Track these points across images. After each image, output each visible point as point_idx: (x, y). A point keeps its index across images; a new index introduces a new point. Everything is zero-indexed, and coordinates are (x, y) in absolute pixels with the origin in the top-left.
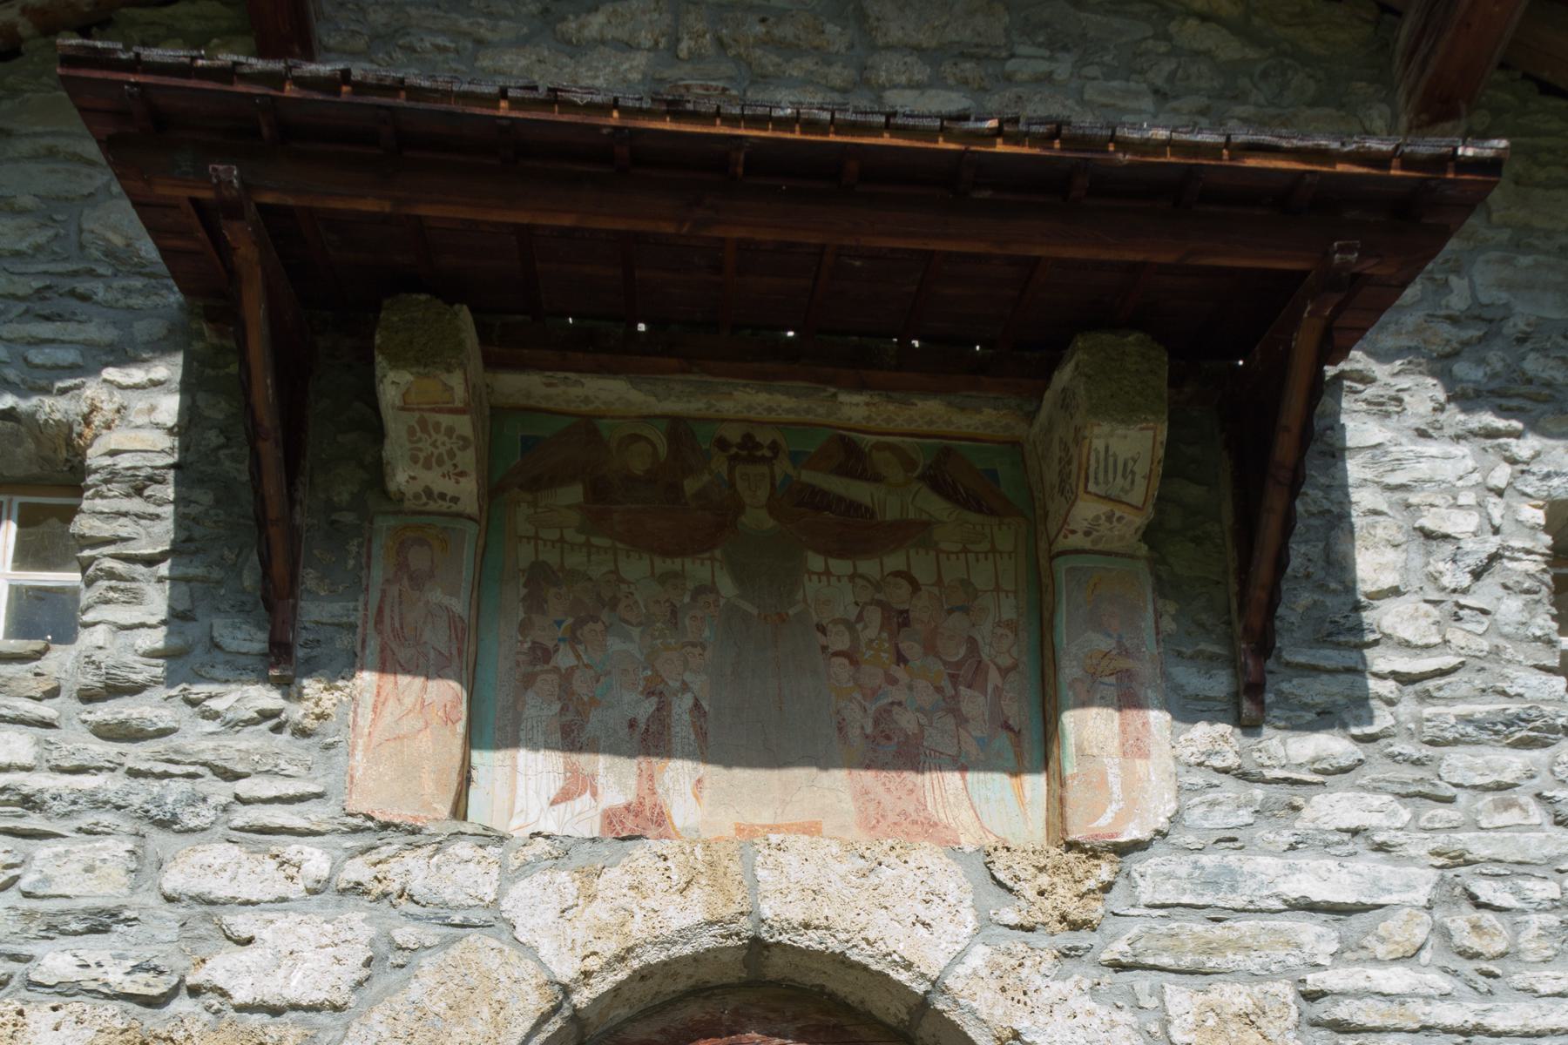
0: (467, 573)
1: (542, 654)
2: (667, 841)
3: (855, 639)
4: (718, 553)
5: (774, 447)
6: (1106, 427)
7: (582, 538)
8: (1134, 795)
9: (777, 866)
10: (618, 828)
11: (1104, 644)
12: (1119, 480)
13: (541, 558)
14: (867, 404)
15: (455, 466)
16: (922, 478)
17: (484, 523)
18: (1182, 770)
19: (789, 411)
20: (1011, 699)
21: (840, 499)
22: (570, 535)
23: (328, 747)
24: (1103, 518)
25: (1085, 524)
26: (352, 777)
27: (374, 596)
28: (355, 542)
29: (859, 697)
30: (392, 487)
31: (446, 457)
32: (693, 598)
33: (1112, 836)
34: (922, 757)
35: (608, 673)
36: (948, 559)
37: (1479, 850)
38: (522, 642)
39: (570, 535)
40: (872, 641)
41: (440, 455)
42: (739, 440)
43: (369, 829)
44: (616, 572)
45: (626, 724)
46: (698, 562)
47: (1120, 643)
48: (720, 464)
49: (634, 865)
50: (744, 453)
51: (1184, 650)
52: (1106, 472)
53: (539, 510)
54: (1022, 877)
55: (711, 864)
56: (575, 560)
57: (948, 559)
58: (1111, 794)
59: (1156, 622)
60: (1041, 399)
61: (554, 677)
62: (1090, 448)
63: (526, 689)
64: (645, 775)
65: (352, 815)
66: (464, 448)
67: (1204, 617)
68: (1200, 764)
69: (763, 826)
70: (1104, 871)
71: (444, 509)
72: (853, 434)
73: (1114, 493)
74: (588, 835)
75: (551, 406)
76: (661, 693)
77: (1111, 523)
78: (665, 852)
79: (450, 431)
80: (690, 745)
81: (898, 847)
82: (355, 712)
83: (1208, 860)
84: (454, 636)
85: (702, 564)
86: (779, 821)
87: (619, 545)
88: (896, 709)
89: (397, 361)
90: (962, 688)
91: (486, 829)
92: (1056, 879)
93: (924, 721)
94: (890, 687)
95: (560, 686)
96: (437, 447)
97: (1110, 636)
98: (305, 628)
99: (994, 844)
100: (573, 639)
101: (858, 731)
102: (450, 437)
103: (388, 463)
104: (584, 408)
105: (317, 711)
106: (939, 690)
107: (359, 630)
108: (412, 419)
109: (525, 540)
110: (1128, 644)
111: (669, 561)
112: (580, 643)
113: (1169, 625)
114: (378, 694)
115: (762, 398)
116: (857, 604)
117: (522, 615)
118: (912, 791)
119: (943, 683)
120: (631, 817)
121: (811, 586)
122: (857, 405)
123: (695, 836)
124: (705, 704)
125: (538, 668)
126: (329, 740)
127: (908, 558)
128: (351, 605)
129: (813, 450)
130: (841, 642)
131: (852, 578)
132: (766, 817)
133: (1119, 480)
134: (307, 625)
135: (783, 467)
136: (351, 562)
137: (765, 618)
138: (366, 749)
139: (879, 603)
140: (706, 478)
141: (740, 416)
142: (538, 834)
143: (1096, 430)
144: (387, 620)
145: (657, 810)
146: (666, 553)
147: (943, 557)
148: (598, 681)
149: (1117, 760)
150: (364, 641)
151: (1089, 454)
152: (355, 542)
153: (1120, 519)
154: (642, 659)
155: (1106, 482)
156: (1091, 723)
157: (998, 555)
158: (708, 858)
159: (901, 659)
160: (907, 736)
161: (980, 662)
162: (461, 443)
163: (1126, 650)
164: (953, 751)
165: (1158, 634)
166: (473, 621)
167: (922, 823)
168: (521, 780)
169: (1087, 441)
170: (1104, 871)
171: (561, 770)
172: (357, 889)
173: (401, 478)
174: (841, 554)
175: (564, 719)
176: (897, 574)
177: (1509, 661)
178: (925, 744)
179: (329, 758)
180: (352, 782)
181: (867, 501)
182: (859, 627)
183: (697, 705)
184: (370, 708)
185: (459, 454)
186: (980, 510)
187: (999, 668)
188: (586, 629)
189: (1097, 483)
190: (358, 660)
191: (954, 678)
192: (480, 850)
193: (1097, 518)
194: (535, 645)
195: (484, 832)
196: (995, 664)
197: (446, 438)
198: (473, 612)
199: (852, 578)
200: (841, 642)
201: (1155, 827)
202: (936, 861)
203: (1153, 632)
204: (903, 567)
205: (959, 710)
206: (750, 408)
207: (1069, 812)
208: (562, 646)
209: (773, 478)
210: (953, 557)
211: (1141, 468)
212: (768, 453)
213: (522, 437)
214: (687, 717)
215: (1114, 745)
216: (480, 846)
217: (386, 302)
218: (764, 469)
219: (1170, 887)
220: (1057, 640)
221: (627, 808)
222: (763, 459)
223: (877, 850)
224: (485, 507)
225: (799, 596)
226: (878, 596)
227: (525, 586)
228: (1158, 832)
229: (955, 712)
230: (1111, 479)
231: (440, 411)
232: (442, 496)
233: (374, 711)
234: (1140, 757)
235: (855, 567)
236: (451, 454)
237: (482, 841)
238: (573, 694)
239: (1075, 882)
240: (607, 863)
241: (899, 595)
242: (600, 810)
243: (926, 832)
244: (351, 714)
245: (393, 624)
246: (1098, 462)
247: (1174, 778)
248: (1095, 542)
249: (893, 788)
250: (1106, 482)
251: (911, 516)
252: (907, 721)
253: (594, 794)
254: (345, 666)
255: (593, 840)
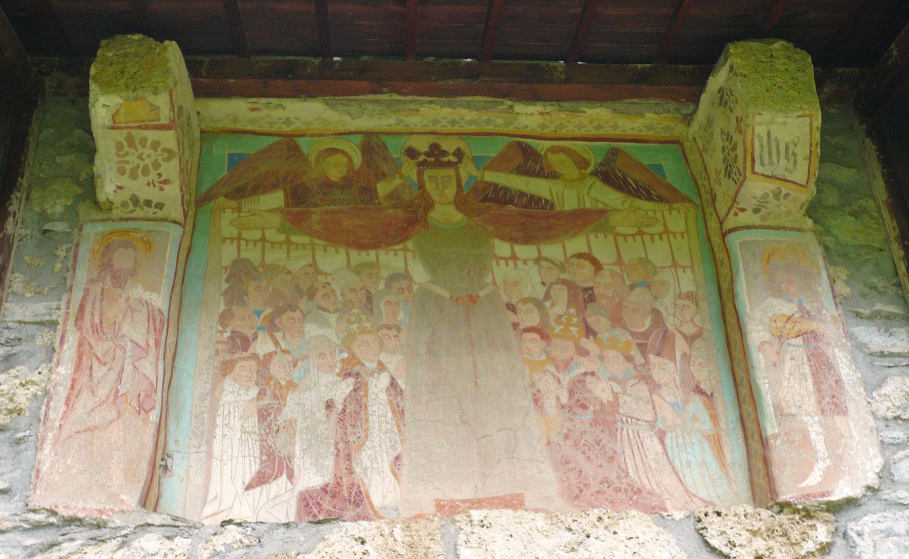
0: (169, 270)
1: (241, 342)
2: (365, 523)
3: (544, 315)
4: (410, 244)
5: (459, 153)
6: (766, 116)
7: (282, 237)
8: (839, 451)
9: (481, 543)
10: (315, 510)
11: (788, 308)
12: (783, 161)
13: (243, 256)
14: (541, 114)
15: (160, 175)
16: (595, 174)
17: (189, 227)
18: (881, 425)
19: (471, 122)
20: (700, 364)
21: (522, 194)
22: (271, 235)
23: (18, 442)
24: (771, 195)
25: (755, 202)
26: (38, 471)
27: (77, 296)
28: (64, 247)
29: (553, 369)
30: (101, 197)
31: (151, 168)
32: (388, 286)
33: (823, 495)
34: (619, 424)
35: (305, 357)
36: (626, 241)
38: (222, 333)
39: (271, 235)
40: (560, 317)
41: (146, 166)
42: (426, 149)
43: (52, 524)
44: (314, 265)
45: (323, 406)
46: (392, 253)
47: (801, 307)
48: (410, 170)
49: (329, 550)
50: (432, 159)
51: (861, 310)
52: (770, 154)
53: (242, 215)
54: (737, 543)
55: (411, 546)
56: (274, 257)
57: (626, 241)
58: (816, 452)
59: (832, 287)
60: (696, 101)
61: (253, 363)
62: (753, 135)
63: (224, 376)
64: (342, 455)
65: (34, 511)
66: (168, 159)
67: (875, 280)
68: (897, 418)
69: (464, 501)
70: (822, 533)
71: (150, 215)
72: (530, 141)
73: (780, 173)
74: (284, 520)
75: (256, 128)
76: (358, 374)
77: (778, 199)
78: (362, 535)
79: (155, 145)
80: (387, 422)
81: (605, 518)
82: (48, 406)
84: (152, 328)
85: (396, 255)
86: (481, 495)
87: (317, 241)
88: (589, 378)
89: (108, 87)
90: (651, 357)
91: (176, 519)
92: (771, 543)
93: (618, 389)
94: (581, 359)
95: (258, 372)
96: (143, 160)
97: (790, 301)
98: (8, 328)
99: (704, 510)
100: (271, 327)
101: (553, 402)
102: (156, 150)
103: (99, 176)
104: (286, 129)
105: (11, 406)
106: (629, 359)
107: (59, 327)
108: (121, 136)
109: (228, 241)
110: (808, 307)
111: (364, 253)
112: (278, 330)
113: (843, 289)
114: (72, 387)
115: (446, 112)
116: (543, 284)
117: (222, 307)
118: (612, 458)
119: (632, 353)
120: (328, 498)
121: (500, 271)
122: (532, 114)
123: (394, 515)
124: (401, 383)
125: (237, 355)
126: (20, 435)
127: (588, 242)
128: (54, 304)
129: (493, 155)
130: (531, 319)
131: (537, 261)
132: (467, 492)
133: (783, 161)
134: (10, 325)
135: (467, 170)
136: (58, 266)
137: (457, 300)
138: (56, 440)
139: (565, 282)
140: (397, 181)
141: (427, 129)
142: (230, 522)
143: (758, 118)
144: (87, 316)
145: (355, 490)
146: (361, 246)
147: (620, 240)
148: (295, 366)
149: (816, 419)
150: (63, 338)
151: (753, 140)
152: (64, 247)
153: (787, 195)
154: (339, 342)
155: (771, 164)
156: (785, 383)
157: (671, 236)
158: (408, 539)
159: (589, 332)
160: (602, 404)
161: (666, 331)
162: (166, 155)
163: (808, 313)
164: (649, 416)
165: (834, 297)
166: (174, 314)
167: (626, 491)
168: (215, 463)
169: (750, 128)
170: (822, 533)
171: (258, 454)
173: (107, 190)
174: (527, 240)
175: (261, 403)
176: (580, 256)
178: (621, 411)
179: (18, 453)
180: (37, 477)
181: (546, 195)
182: (548, 304)
183: (393, 384)
184: (62, 402)
185: (164, 165)
186: (650, 198)
187: (685, 337)
188: (284, 317)
189: (763, 165)
190: (55, 355)
191: (642, 347)
192: (167, 542)
193: (766, 195)
194: (235, 335)
195: (173, 523)
196: (680, 332)
197: (152, 152)
198: (174, 307)
199: (537, 261)
200: (531, 319)
201: (865, 483)
202: (646, 530)
203: (830, 296)
204: (585, 250)
205: (651, 377)
206: (436, 122)
207: (776, 472)
208: (261, 334)
209: (459, 179)
210: (630, 239)
211: (802, 151)
212: (453, 159)
213: (229, 154)
214: (383, 396)
215: (810, 403)
216: (168, 538)
217: (103, 42)
218: (450, 172)
219: (891, 545)
220: (740, 308)
221: (324, 489)
222: (449, 164)
223: (584, 521)
224: (191, 213)
225: (489, 279)
226: (563, 276)
227: (227, 281)
228: (869, 488)
229: (647, 379)
230: (775, 161)
231: (147, 128)
232: (148, 203)
233: (67, 403)
234: (839, 413)
235: (539, 252)
236: (156, 165)
237: (169, 532)
238: (270, 379)
239: (793, 544)
240: (301, 549)
241: (583, 274)
242: (296, 493)
243: (631, 499)
244: (44, 408)
245: (92, 320)
246: (762, 146)
247: (875, 432)
248: (763, 218)
249: (592, 456)
250: (771, 164)
251: (588, 205)
252: (601, 390)
253: (291, 477)
254: (44, 362)
255: (287, 525)
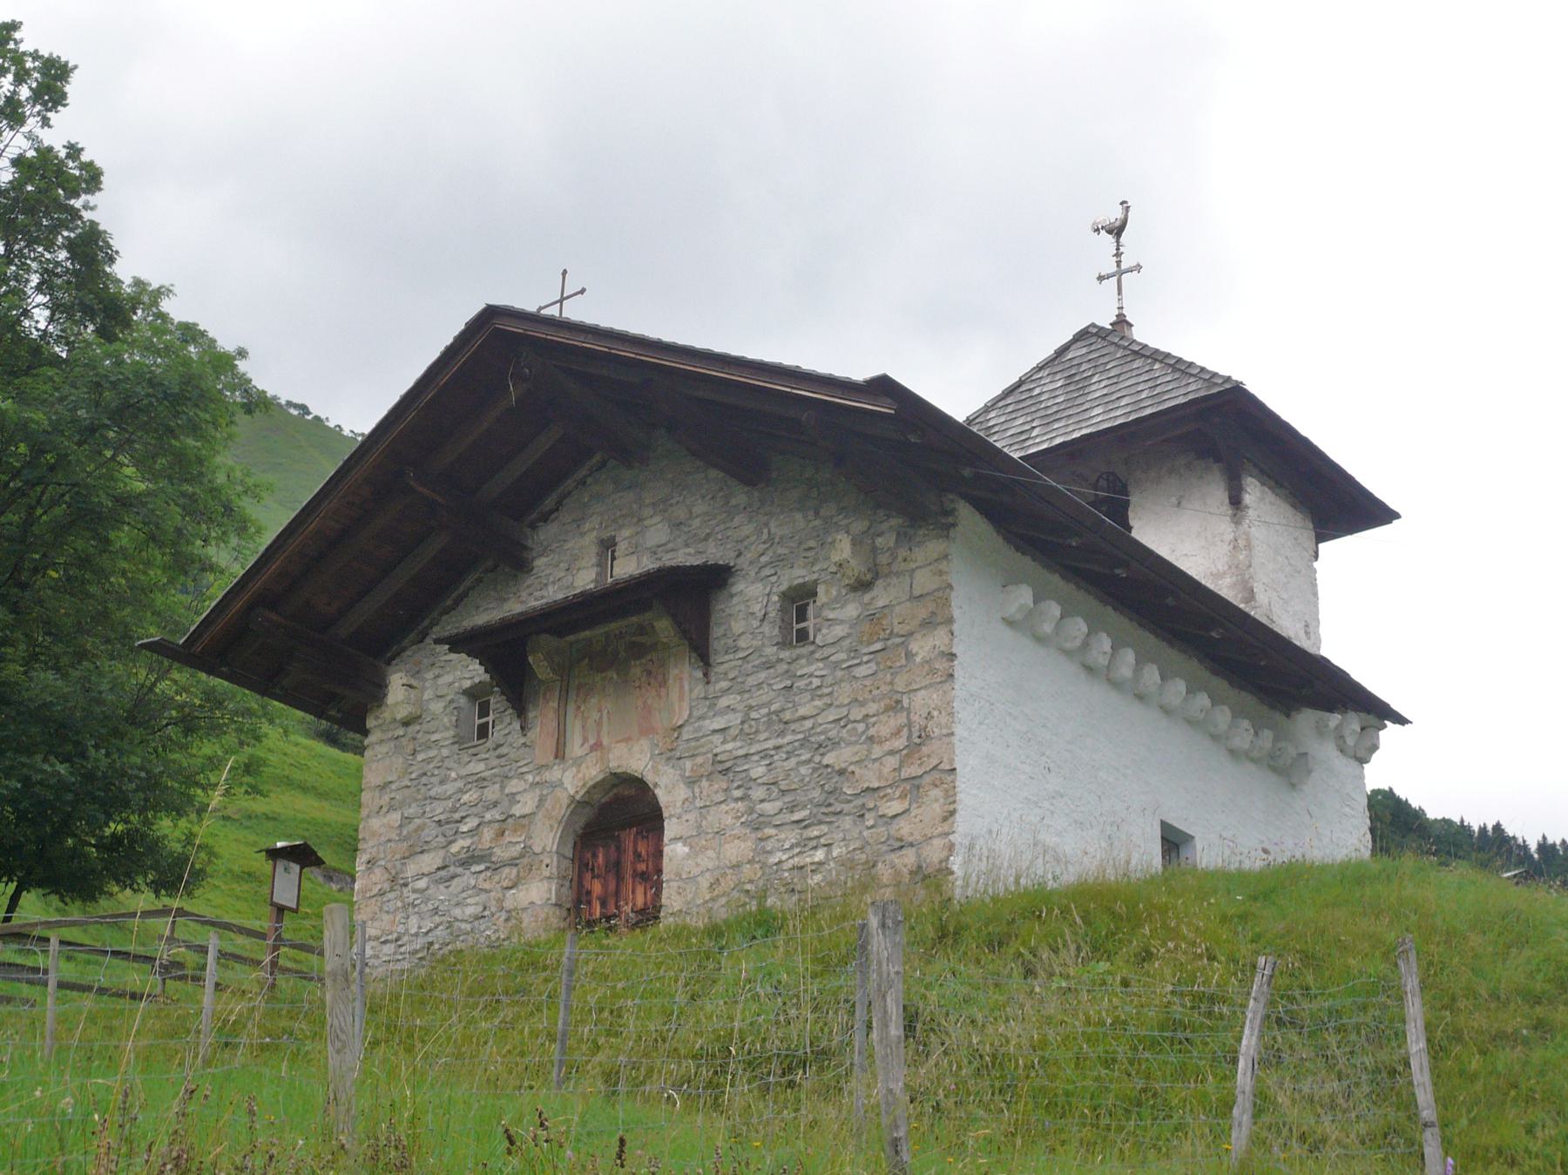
1: (579, 707)
37: (754, 704)
83: (696, 725)
113: (693, 660)
130: (637, 684)
172: (538, 783)
177: (10, 660)
